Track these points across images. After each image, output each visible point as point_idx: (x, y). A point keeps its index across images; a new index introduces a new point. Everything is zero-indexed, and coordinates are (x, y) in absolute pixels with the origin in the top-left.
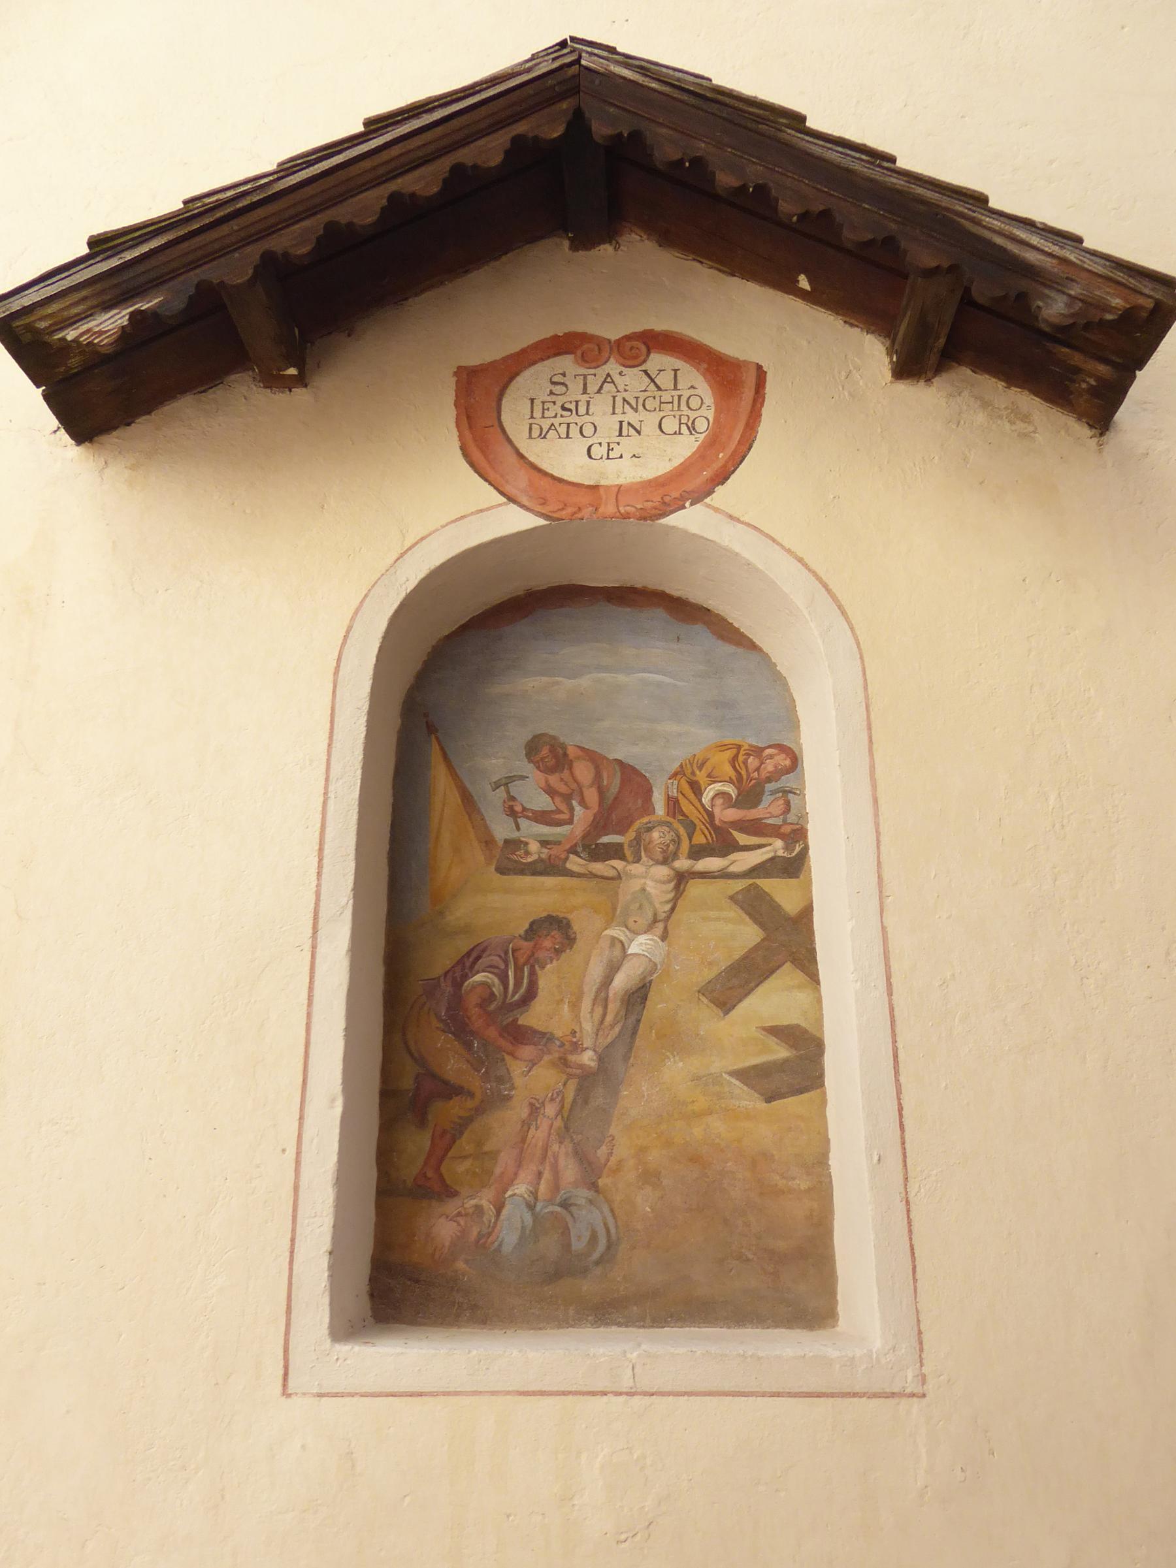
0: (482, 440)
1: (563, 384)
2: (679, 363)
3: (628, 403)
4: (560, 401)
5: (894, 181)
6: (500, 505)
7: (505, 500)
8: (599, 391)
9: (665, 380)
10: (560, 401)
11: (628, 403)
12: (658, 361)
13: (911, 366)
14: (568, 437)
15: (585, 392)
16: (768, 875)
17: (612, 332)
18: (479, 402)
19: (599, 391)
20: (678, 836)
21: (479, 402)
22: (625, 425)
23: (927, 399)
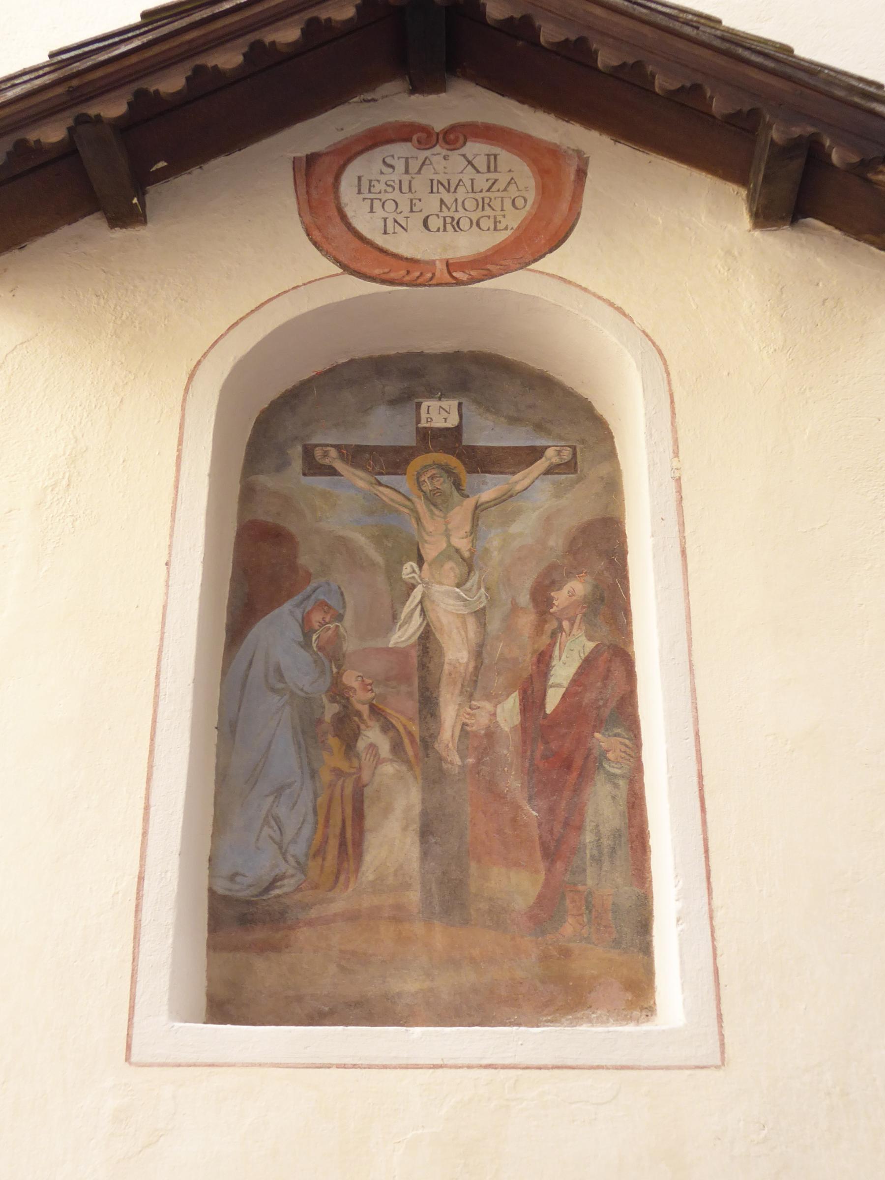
0: (324, 220)
1: (392, 186)
2: (496, 150)
3: (442, 184)
4: (387, 177)
5: (766, 156)
6: (337, 275)
7: (340, 271)
8: (419, 172)
9: (481, 162)
10: (387, 177)
11: (442, 184)
12: (476, 149)
13: (765, 216)
14: (394, 233)
15: (407, 172)
16: (515, 451)
17: (439, 126)
18: (316, 178)
19: (419, 172)
20: (440, 466)
21: (316, 178)
22: (435, 183)
23: (781, 247)
